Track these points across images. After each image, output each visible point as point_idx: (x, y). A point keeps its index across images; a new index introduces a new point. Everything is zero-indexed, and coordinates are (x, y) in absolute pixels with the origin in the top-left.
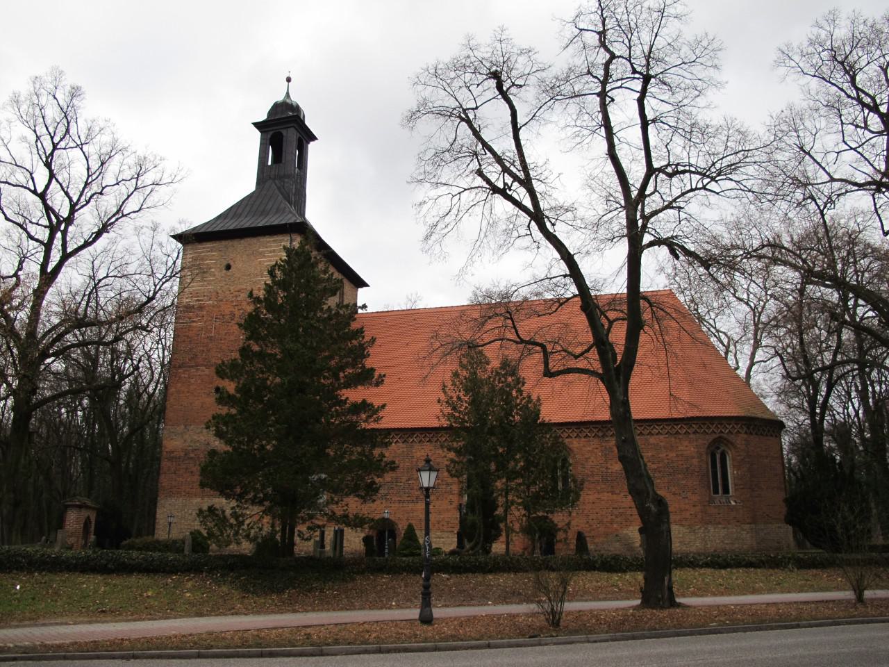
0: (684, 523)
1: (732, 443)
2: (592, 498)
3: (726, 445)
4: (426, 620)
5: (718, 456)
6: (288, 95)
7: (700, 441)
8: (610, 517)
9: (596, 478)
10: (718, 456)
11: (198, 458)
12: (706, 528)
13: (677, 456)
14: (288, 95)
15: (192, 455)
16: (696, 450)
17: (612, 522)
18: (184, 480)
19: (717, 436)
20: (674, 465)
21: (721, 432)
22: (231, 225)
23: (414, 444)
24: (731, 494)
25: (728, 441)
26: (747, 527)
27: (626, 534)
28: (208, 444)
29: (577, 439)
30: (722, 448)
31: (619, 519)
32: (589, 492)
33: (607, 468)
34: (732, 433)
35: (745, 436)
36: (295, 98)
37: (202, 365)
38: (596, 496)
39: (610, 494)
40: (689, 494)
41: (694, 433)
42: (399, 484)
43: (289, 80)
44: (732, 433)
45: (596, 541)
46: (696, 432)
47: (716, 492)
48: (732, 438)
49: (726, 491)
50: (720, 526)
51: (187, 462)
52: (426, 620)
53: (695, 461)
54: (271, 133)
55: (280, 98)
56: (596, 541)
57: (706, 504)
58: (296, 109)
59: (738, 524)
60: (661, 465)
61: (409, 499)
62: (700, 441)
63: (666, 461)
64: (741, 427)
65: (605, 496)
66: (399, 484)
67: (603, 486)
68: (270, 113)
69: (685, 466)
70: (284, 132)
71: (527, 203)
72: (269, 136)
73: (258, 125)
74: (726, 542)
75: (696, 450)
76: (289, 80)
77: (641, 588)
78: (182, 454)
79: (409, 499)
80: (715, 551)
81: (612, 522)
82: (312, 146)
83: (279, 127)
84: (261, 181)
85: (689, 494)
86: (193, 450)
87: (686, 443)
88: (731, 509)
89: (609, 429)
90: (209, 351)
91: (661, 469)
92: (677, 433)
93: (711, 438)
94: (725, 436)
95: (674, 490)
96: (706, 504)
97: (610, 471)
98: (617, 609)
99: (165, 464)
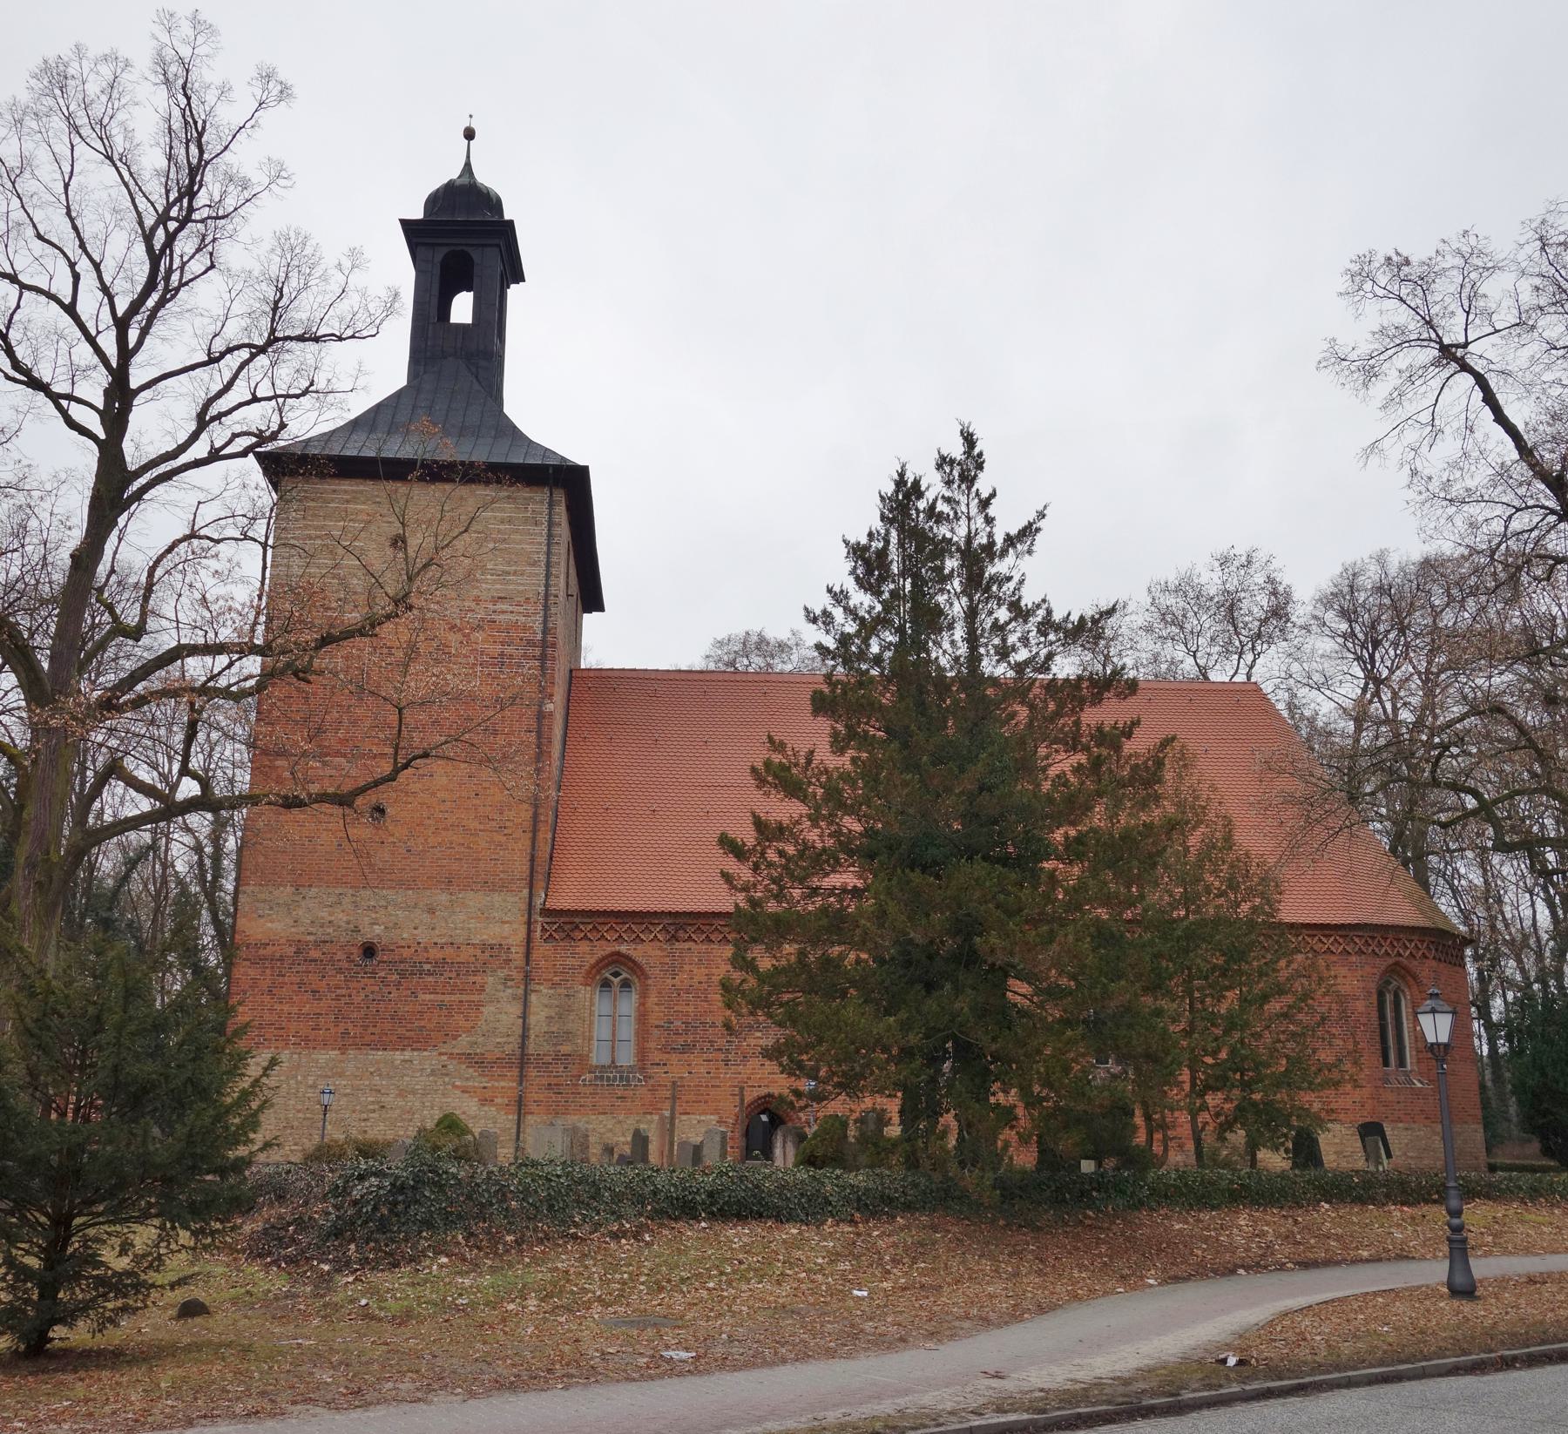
1: (1415, 978)
3: (1403, 978)
4: (1463, 1290)
5: (1389, 998)
6: (468, 167)
14: (468, 167)
15: (314, 954)
16: (1361, 985)
19: (1391, 961)
22: (363, 447)
24: (1409, 1068)
25: (1408, 971)
28: (356, 930)
30: (624, 975)
34: (1426, 958)
35: (1434, 963)
36: (484, 177)
37: (338, 754)
43: (469, 134)
44: (1426, 958)
46: (1361, 952)
47: (1386, 1063)
49: (1401, 1062)
50: (1401, 1125)
52: (1463, 1290)
54: (445, 250)
55: (453, 172)
57: (1379, 1083)
58: (491, 203)
59: (1427, 1122)
62: (1367, 968)
64: (1428, 948)
68: (433, 201)
70: (476, 255)
72: (439, 257)
74: (1410, 1154)
75: (1361, 985)
76: (469, 134)
78: (291, 951)
82: (514, 291)
83: (463, 241)
88: (1417, 1093)
89: (577, 927)
90: (354, 723)
93: (1383, 964)
94: (1405, 962)
96: (1379, 1083)
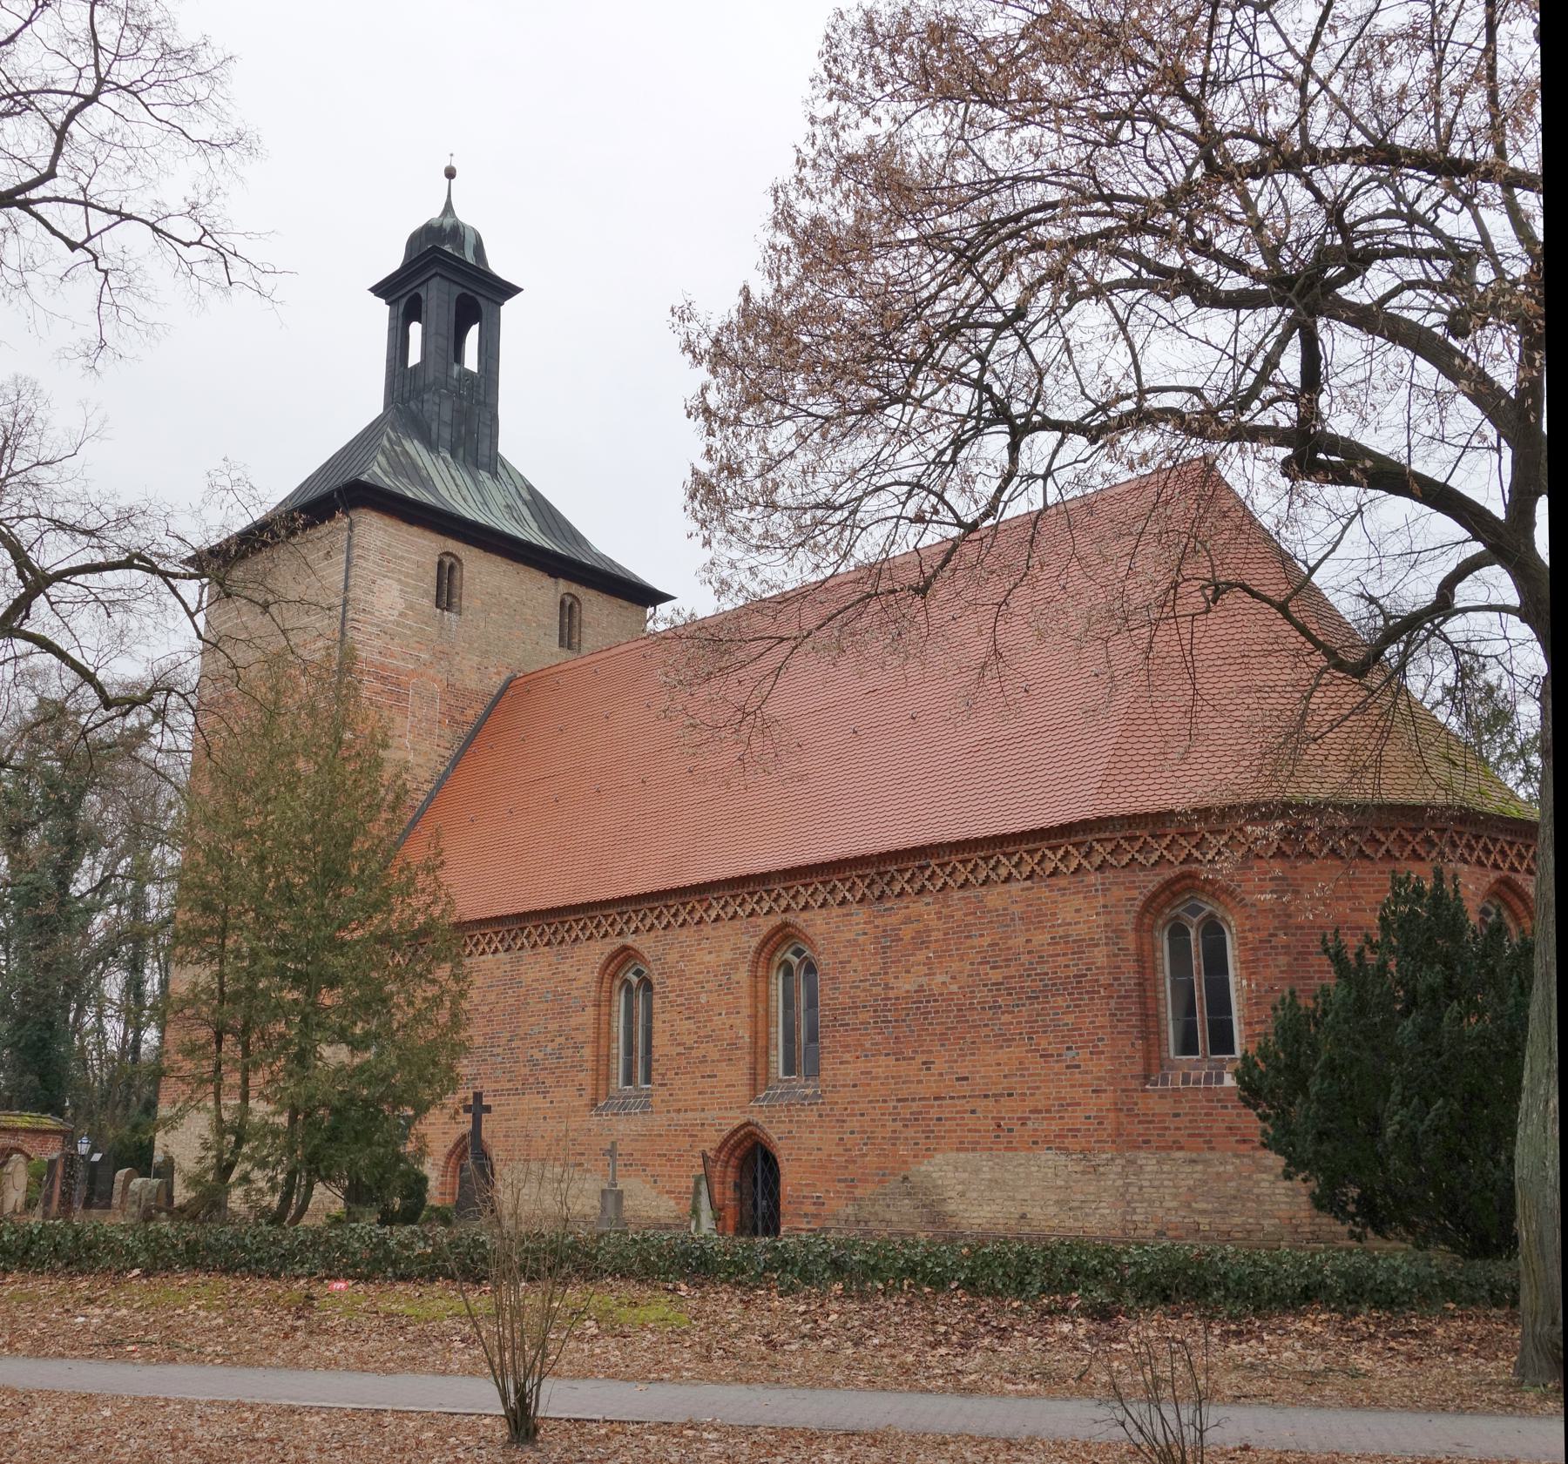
0: (1068, 1142)
2: (851, 1071)
6: (448, 208)
7: (1118, 892)
8: (890, 1125)
9: (864, 1016)
12: (1132, 1162)
13: (1054, 942)
14: (448, 208)
16: (1102, 920)
17: (894, 1140)
20: (1046, 968)
21: (1189, 858)
23: (523, 953)
27: (928, 1175)
29: (824, 911)
31: (910, 1133)
32: (847, 1057)
33: (887, 987)
38: (861, 1065)
39: (891, 1061)
40: (1084, 1054)
41: (1099, 868)
43: (450, 174)
45: (858, 1192)
50: (1180, 1154)
53: (1100, 956)
54: (404, 300)
56: (858, 1192)
58: (456, 233)
60: (1012, 971)
63: (1024, 958)
65: (883, 1066)
66: (496, 1050)
67: (878, 1038)
69: (1074, 971)
73: (510, 290)
75: (1102, 920)
76: (450, 174)
80: (1160, 1234)
81: (894, 1140)
84: (386, 407)
85: (1084, 1054)
87: (1078, 901)
91: (1014, 983)
92: (1055, 873)
95: (1044, 1044)
97: (891, 994)
98: (1321, 1406)
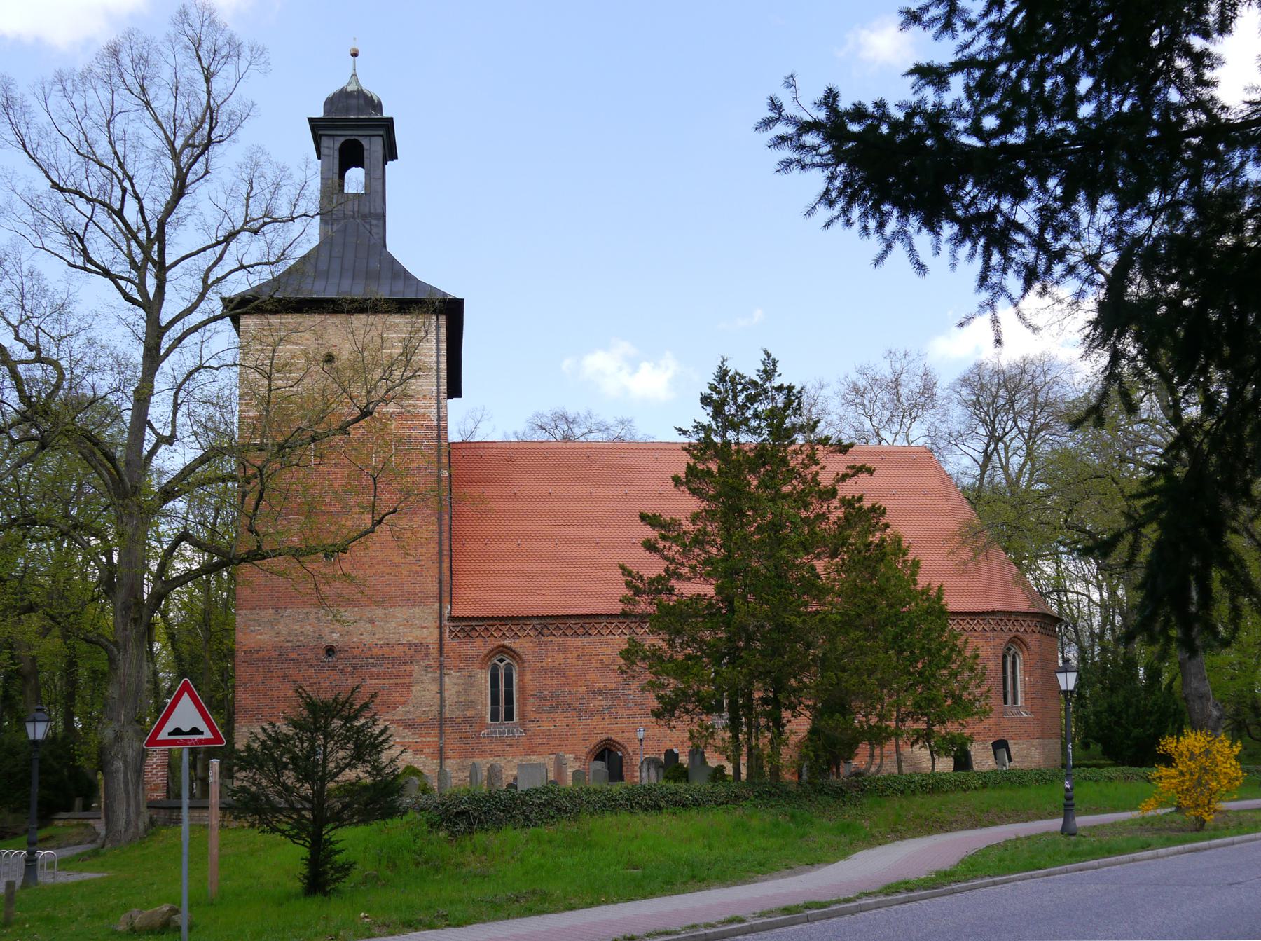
3: (1019, 645)
5: (1009, 659)
10: (502, 672)
11: (305, 658)
15: (293, 656)
18: (282, 695)
19: (1012, 635)
26: (1036, 742)
28: (320, 637)
30: (507, 661)
36: (371, 87)
42: (626, 692)
48: (1026, 637)
51: (285, 665)
54: (342, 139)
61: (642, 712)
62: (997, 640)
66: (626, 692)
68: (330, 103)
70: (365, 142)
71: (123, 283)
75: (993, 651)
77: (332, 843)
79: (642, 712)
86: (294, 648)
88: (1023, 720)
99: (243, 670)
